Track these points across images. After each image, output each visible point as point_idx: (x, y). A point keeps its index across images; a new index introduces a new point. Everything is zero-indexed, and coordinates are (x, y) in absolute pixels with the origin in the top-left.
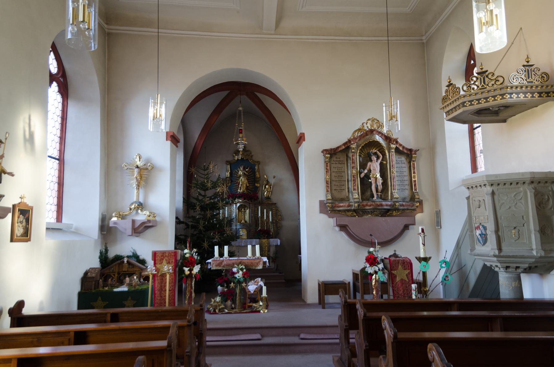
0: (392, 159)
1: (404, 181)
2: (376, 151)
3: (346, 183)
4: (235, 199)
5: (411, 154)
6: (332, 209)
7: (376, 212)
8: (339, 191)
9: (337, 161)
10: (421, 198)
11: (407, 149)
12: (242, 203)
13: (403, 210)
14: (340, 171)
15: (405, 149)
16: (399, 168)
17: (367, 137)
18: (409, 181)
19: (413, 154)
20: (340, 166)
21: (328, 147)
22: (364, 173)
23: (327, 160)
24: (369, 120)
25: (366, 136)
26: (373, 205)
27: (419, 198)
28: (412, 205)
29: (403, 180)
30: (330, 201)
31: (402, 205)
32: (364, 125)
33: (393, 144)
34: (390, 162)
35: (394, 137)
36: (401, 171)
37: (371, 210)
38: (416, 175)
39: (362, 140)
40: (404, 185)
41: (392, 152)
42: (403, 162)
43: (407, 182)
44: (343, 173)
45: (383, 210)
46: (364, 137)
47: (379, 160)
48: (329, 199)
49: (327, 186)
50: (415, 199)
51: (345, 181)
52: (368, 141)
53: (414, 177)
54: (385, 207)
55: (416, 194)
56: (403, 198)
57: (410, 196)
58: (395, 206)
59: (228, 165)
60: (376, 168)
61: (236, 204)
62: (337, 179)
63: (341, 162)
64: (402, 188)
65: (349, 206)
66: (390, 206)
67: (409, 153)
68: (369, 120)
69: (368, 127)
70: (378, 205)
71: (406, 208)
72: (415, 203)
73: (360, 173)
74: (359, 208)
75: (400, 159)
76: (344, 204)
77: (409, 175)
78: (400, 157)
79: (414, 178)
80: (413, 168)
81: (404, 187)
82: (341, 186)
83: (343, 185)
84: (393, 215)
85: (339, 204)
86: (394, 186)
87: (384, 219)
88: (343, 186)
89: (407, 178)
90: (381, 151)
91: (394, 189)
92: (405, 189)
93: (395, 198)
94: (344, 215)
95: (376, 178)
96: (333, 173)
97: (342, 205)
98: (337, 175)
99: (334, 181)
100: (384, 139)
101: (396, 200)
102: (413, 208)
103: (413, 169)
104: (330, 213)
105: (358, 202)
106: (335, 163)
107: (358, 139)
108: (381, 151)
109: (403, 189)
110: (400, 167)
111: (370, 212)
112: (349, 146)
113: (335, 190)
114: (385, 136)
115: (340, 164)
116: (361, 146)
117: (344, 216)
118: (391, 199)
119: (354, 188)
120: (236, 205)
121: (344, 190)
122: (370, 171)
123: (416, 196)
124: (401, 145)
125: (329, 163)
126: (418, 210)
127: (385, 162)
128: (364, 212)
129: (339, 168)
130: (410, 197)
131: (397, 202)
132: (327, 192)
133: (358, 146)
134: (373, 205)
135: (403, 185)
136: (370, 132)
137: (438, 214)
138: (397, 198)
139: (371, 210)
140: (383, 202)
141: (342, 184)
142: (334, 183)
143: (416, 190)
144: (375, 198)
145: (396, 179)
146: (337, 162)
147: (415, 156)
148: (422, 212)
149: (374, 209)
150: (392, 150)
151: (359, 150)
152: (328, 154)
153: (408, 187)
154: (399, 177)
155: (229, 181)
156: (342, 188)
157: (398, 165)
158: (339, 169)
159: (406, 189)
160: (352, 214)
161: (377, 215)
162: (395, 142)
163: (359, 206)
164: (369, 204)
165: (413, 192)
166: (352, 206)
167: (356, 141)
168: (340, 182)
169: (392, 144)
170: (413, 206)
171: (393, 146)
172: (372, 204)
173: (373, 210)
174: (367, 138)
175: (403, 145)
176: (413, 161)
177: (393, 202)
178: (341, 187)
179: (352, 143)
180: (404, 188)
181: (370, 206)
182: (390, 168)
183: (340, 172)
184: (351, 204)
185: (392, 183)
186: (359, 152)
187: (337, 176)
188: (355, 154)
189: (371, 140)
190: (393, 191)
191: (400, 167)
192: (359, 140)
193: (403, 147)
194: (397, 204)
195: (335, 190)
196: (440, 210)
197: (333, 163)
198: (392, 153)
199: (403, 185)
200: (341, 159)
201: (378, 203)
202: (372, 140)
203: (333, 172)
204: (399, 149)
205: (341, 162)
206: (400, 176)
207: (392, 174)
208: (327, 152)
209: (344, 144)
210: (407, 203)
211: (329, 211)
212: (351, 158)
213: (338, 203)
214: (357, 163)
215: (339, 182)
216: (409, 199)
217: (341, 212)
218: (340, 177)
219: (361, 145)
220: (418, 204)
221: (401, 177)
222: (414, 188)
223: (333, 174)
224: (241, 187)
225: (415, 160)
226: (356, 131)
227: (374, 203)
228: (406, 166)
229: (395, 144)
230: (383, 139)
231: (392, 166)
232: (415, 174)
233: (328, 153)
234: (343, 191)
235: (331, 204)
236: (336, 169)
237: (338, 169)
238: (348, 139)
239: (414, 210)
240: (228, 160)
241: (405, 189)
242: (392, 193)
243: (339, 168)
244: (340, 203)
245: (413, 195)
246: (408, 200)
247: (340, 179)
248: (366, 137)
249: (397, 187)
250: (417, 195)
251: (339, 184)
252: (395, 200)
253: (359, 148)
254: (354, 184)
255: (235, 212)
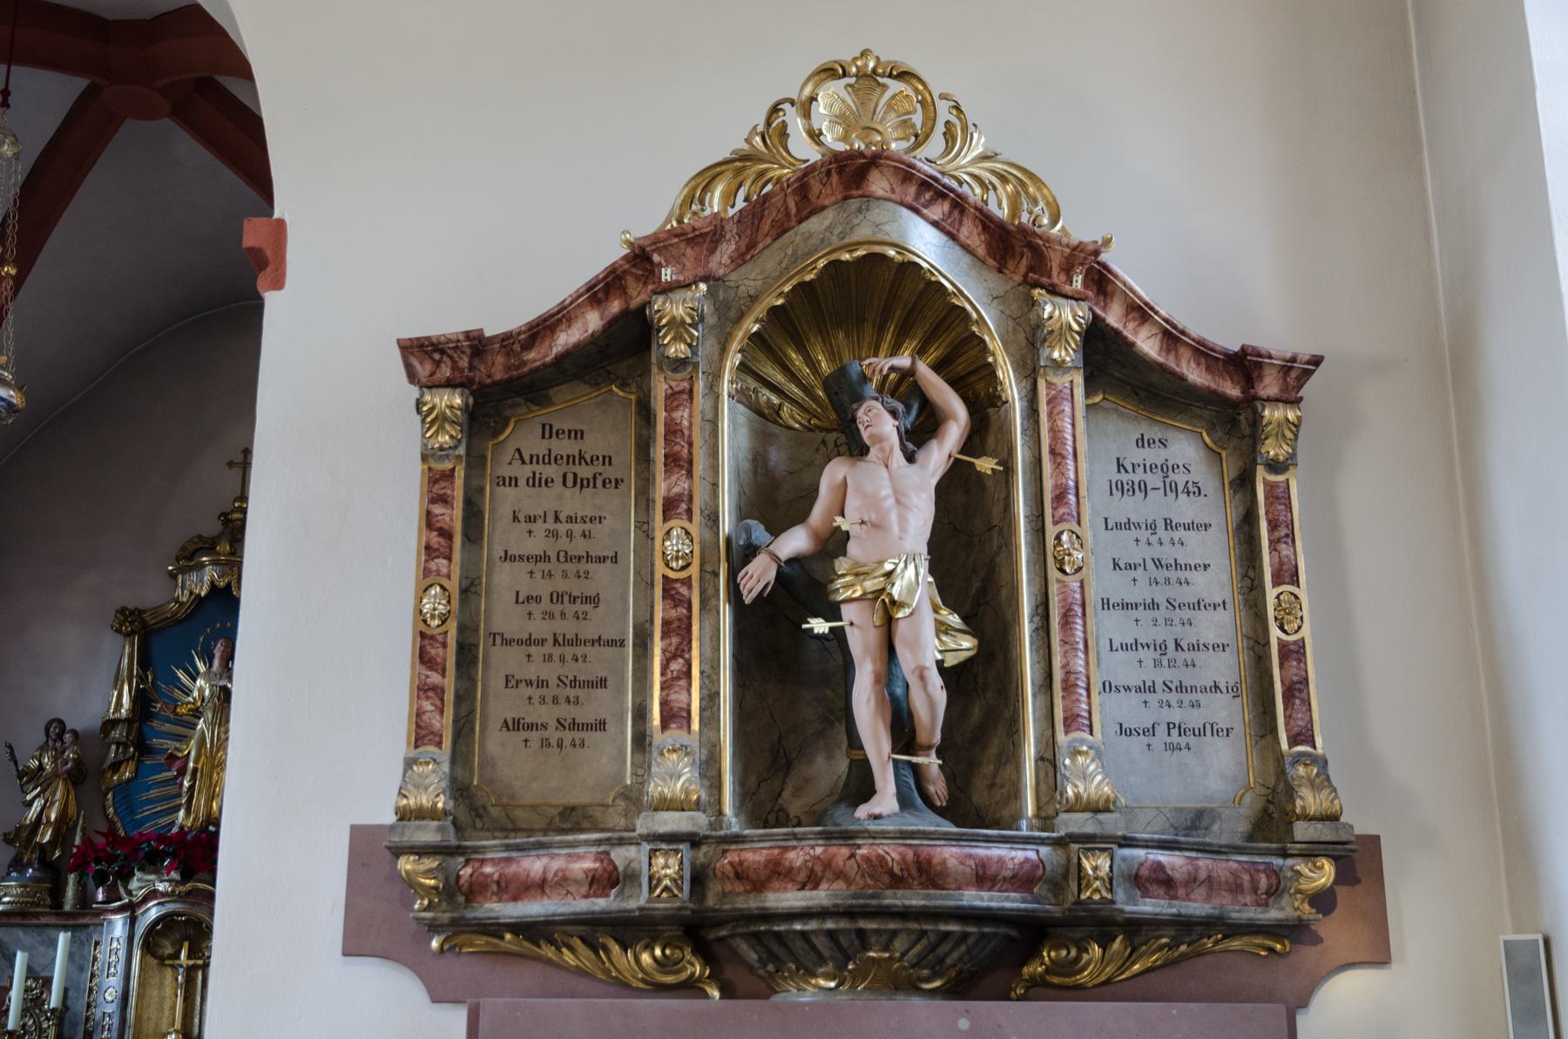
0: (1055, 432)
1: (1188, 656)
2: (903, 361)
3: (624, 661)
4: (126, 876)
5: (1251, 401)
6: (445, 917)
7: (886, 948)
8: (553, 734)
9: (549, 458)
10: (1360, 821)
11: (1204, 353)
12: (171, 907)
13: (1185, 927)
14: (579, 547)
15: (1183, 351)
16: (1144, 534)
17: (815, 224)
18: (1244, 657)
19: (1269, 400)
20: (573, 502)
21: (447, 323)
22: (775, 558)
23: (444, 439)
24: (829, 72)
25: (800, 222)
26: (840, 875)
27: (1333, 818)
28: (1263, 882)
29: (1178, 645)
30: (428, 834)
31: (1162, 881)
32: (784, 125)
33: (1066, 297)
34: (1037, 463)
35: (1076, 227)
36: (1158, 564)
37: (830, 925)
38: (1302, 593)
39: (771, 260)
40: (1193, 689)
41: (1058, 366)
42: (1180, 478)
43: (1225, 667)
44: (601, 572)
45: (953, 927)
46: (781, 230)
47: (934, 444)
48: (420, 814)
49: (423, 690)
50: (1290, 831)
51: (622, 643)
52: (821, 264)
53: (1288, 611)
54: (974, 898)
55: (1301, 770)
56: (1179, 810)
57: (1247, 799)
58: (1074, 886)
59: (133, 633)
60: (893, 517)
61: (131, 909)
62: (540, 628)
63: (585, 472)
64: (1176, 715)
65: (608, 879)
66: (1024, 880)
67: (1233, 391)
68: (829, 72)
69: (815, 136)
70: (891, 873)
71: (1197, 907)
72: (1302, 867)
73: (744, 554)
74: (711, 901)
75: (1153, 455)
76: (557, 864)
77: (1239, 598)
78: (1153, 432)
79: (1282, 628)
80: (1273, 526)
81: (1195, 705)
82: (572, 693)
83: (591, 684)
84: (1079, 987)
85: (508, 860)
86: (1069, 687)
87: (964, 1024)
88: (600, 692)
89: (1220, 626)
90: (961, 367)
91: (1070, 722)
92: (1201, 733)
93: (1080, 805)
94: (580, 972)
95: (887, 612)
96: (507, 565)
97: (534, 865)
98: (543, 588)
99: (507, 642)
100: (981, 251)
101: (1090, 828)
102: (1273, 914)
103: (1274, 543)
104: (441, 950)
105: (694, 840)
106: (535, 481)
107: (727, 250)
108: (961, 367)
109: (1182, 731)
110: (1152, 527)
111: (821, 943)
112: (642, 309)
113: (514, 725)
114: (985, 228)
115: (581, 483)
116: (760, 310)
117: (583, 984)
118: (1045, 820)
119: (664, 703)
120: (133, 921)
121: (601, 725)
122: (834, 543)
123: (1305, 792)
124: (1141, 312)
125: (460, 473)
126: (1335, 931)
127: (986, 465)
128: (775, 947)
129: (563, 528)
130: (1251, 804)
131: (1089, 841)
132: (418, 741)
133: (728, 314)
134: (840, 875)
135: (1181, 688)
136: (835, 178)
137: (1533, 975)
138: (1098, 808)
139: (830, 925)
140: (947, 837)
141: (585, 672)
142: (499, 663)
143: (1303, 736)
144: (885, 801)
145: (1109, 627)
146: (550, 471)
147: (1291, 416)
148: (1380, 956)
149: (850, 913)
150: (1056, 355)
151: (735, 345)
152: (449, 384)
153: (1229, 711)
154: (1140, 613)
155: (126, 746)
156: (587, 714)
157: (1129, 508)
158: (570, 535)
159: (1216, 732)
160: (662, 964)
161: (903, 984)
162: (1078, 282)
163: (699, 879)
164: (796, 858)
165: (1280, 757)
166: (631, 877)
167: (713, 264)
168: (569, 651)
169: (1053, 291)
170: (1275, 892)
171: (1064, 314)
172: (828, 865)
173: (843, 924)
174: (809, 236)
175: (1165, 309)
176: (1275, 466)
177: (1060, 843)
178: (577, 701)
179: (667, 274)
180: (1194, 719)
181: (811, 881)
182: (1038, 531)
183: (569, 558)
184: (620, 855)
185: (1057, 662)
186: (744, 368)
187: (538, 600)
188: (700, 385)
189: (850, 247)
190: (1061, 738)
191: (1152, 527)
192: (740, 259)
193: (1172, 337)
194: (1097, 864)
195: (514, 725)
196: (1547, 942)
197: (514, 481)
198: (1062, 381)
199: (1181, 688)
200: (593, 444)
201: (892, 852)
202: (860, 253)
203: (506, 557)
204: (1132, 344)
205: (585, 472)
206: (1154, 605)
207: (1053, 573)
208: (438, 363)
209: (601, 289)
210: (1205, 863)
211: (433, 928)
212: (661, 416)
213: (508, 848)
214: (715, 468)
215: (557, 651)
216: (1243, 827)
217: (552, 942)
218: (570, 609)
219: (754, 299)
220: (1324, 874)
221: (1163, 613)
222: (1288, 718)
223: (506, 580)
224: (192, 788)
225: (1293, 456)
226: (708, 177)
227: (845, 851)
228: (1216, 520)
229: (1077, 298)
230: (966, 248)
231: (1060, 498)
232: (1297, 583)
233: (446, 371)
234: (585, 735)
235: (431, 863)
236: (539, 528)
237: (554, 534)
238: (630, 244)
239: (1295, 931)
240: (131, 606)
241: (1201, 733)
242: (1049, 761)
243: (570, 519)
244: (519, 848)
245: (1281, 787)
246: (1231, 827)
247: (568, 628)
248: (805, 226)
249: (1105, 710)
250: (1312, 785)
251: (550, 672)
252: (1074, 829)
253: (740, 334)
254: (676, 666)
255: (120, 968)
